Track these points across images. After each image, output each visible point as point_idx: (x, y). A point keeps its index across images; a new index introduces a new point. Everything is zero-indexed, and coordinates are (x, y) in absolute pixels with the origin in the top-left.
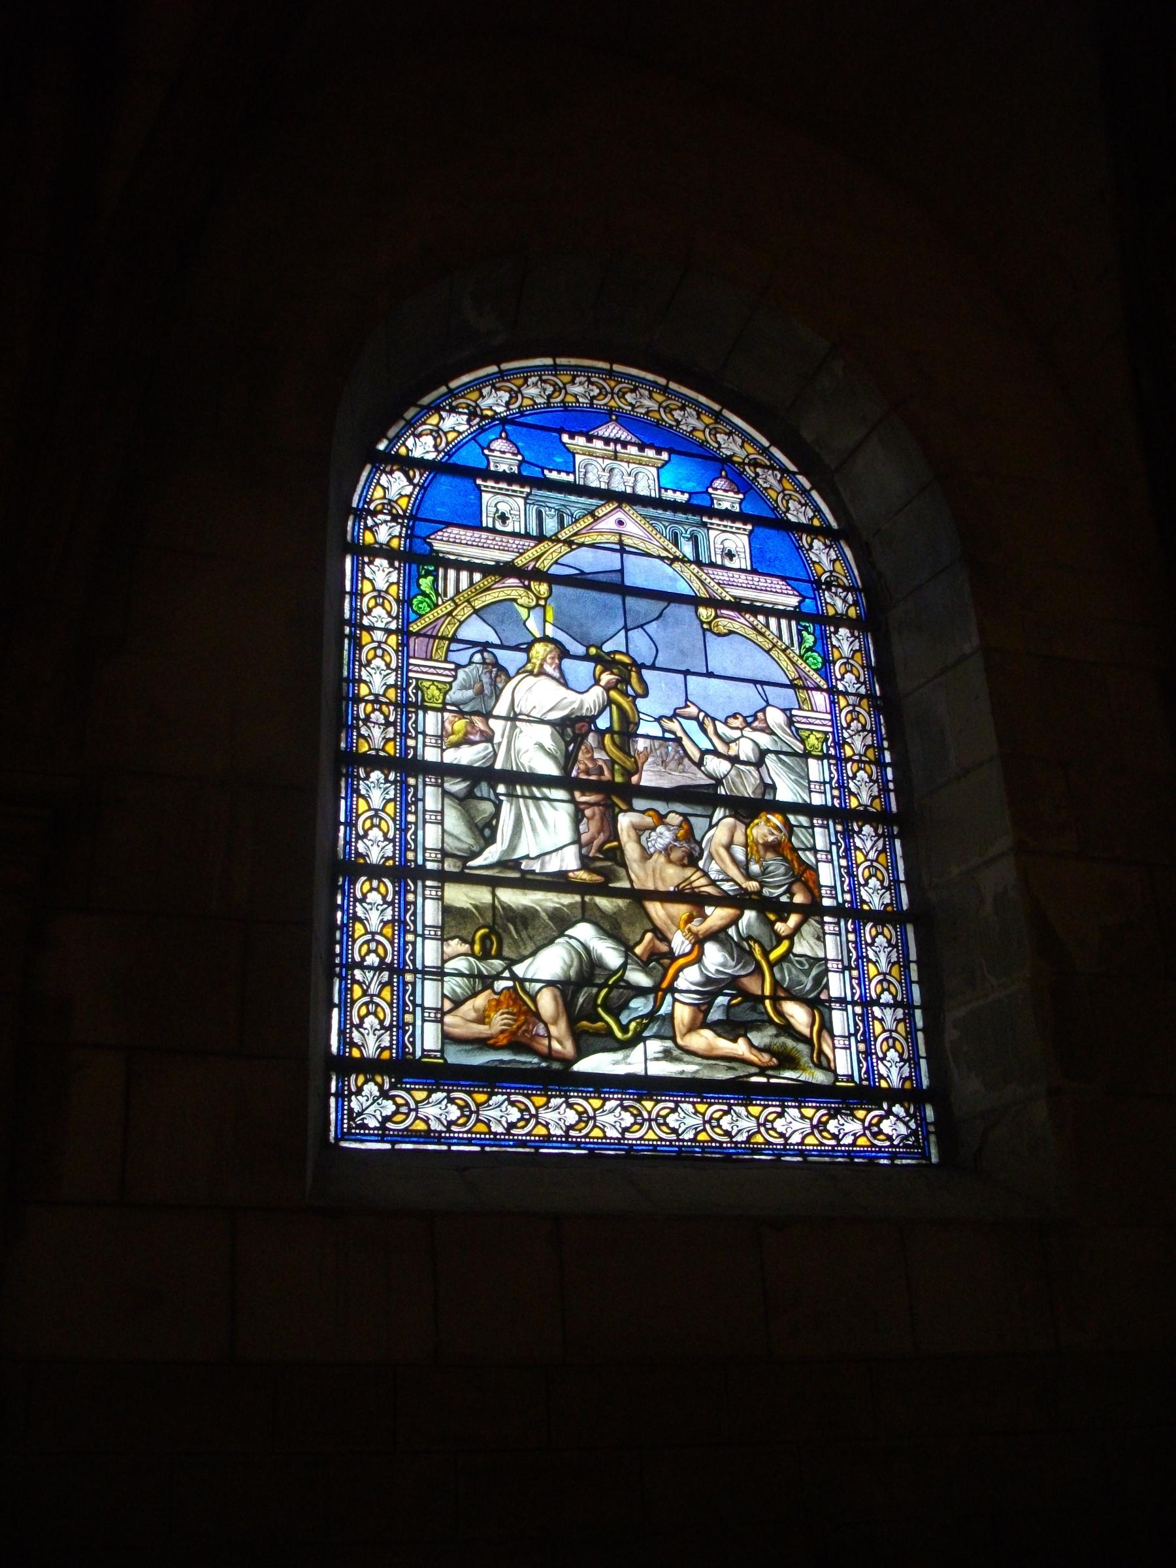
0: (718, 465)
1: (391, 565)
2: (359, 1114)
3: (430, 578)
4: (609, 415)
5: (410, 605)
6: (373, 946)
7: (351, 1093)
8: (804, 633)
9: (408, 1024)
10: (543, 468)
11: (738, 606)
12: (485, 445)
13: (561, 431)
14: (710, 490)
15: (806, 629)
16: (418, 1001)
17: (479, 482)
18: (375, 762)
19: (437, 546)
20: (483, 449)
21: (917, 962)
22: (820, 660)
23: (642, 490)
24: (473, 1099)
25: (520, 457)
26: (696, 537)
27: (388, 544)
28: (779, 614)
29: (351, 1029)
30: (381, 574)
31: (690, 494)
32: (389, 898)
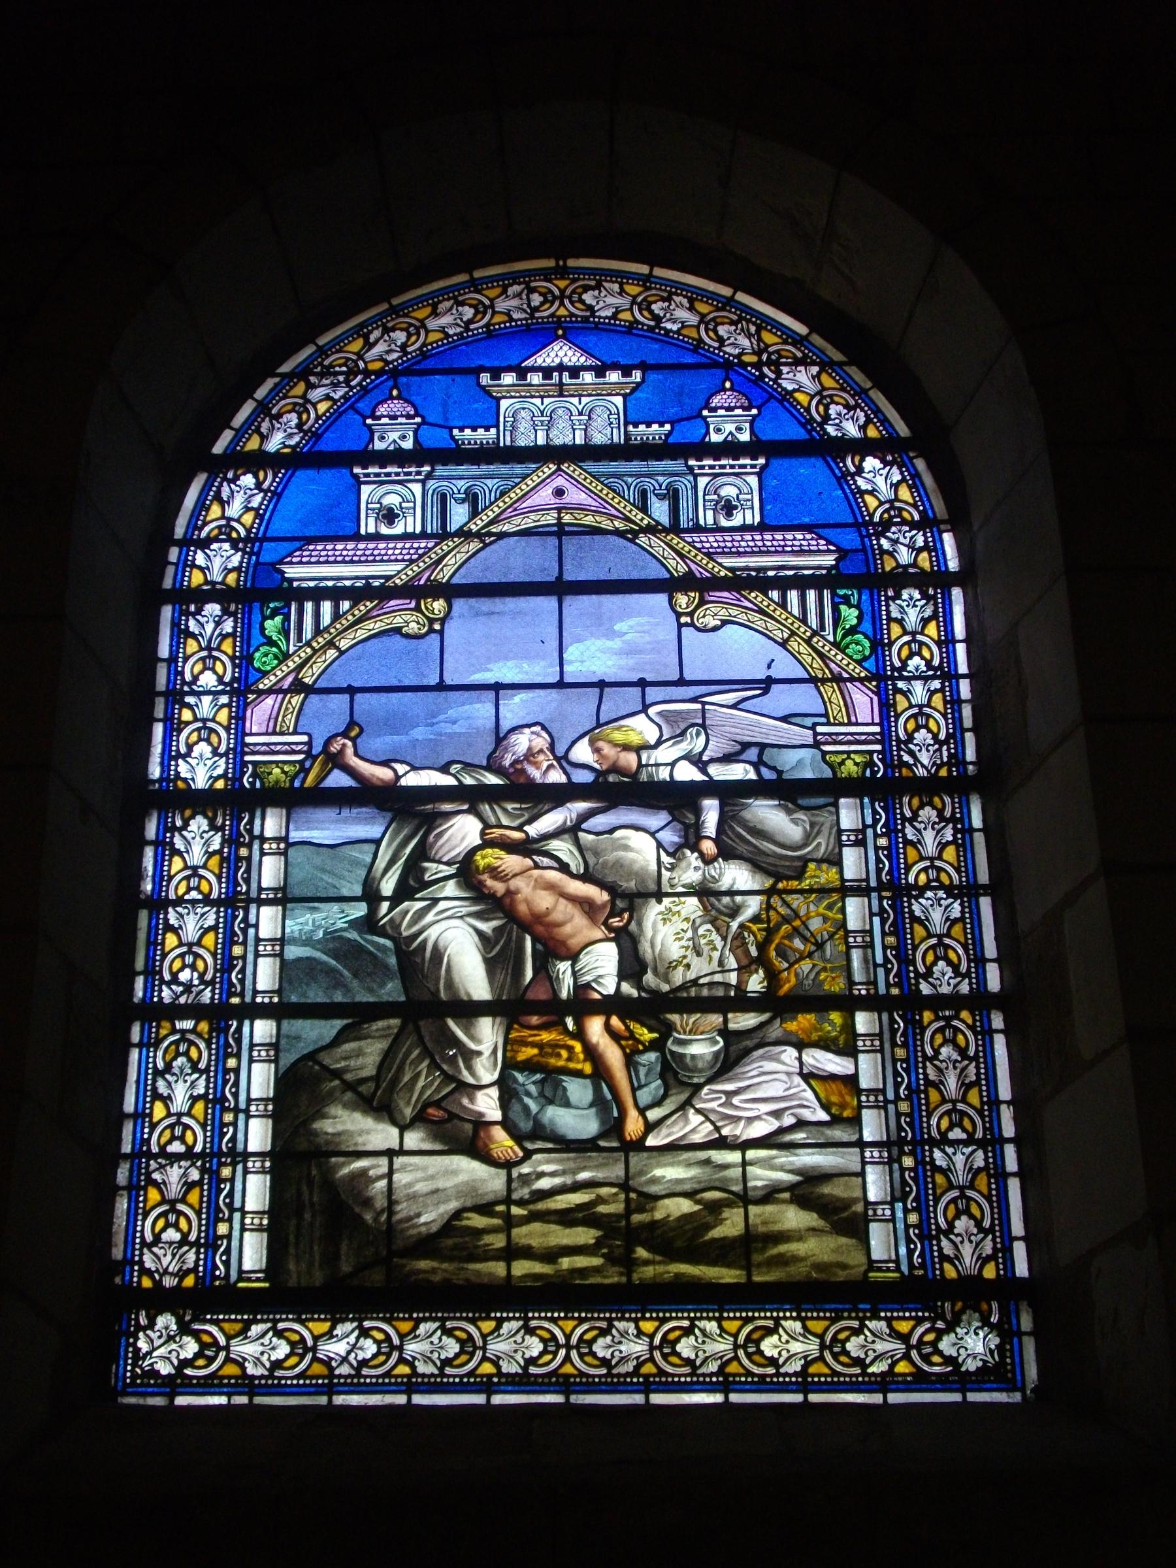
8: (843, 608)
9: (227, 1125)
10: (451, 429)
14: (705, 413)
15: (846, 600)
17: (357, 470)
20: (365, 418)
26: (676, 491)
28: (802, 583)
31: (672, 423)
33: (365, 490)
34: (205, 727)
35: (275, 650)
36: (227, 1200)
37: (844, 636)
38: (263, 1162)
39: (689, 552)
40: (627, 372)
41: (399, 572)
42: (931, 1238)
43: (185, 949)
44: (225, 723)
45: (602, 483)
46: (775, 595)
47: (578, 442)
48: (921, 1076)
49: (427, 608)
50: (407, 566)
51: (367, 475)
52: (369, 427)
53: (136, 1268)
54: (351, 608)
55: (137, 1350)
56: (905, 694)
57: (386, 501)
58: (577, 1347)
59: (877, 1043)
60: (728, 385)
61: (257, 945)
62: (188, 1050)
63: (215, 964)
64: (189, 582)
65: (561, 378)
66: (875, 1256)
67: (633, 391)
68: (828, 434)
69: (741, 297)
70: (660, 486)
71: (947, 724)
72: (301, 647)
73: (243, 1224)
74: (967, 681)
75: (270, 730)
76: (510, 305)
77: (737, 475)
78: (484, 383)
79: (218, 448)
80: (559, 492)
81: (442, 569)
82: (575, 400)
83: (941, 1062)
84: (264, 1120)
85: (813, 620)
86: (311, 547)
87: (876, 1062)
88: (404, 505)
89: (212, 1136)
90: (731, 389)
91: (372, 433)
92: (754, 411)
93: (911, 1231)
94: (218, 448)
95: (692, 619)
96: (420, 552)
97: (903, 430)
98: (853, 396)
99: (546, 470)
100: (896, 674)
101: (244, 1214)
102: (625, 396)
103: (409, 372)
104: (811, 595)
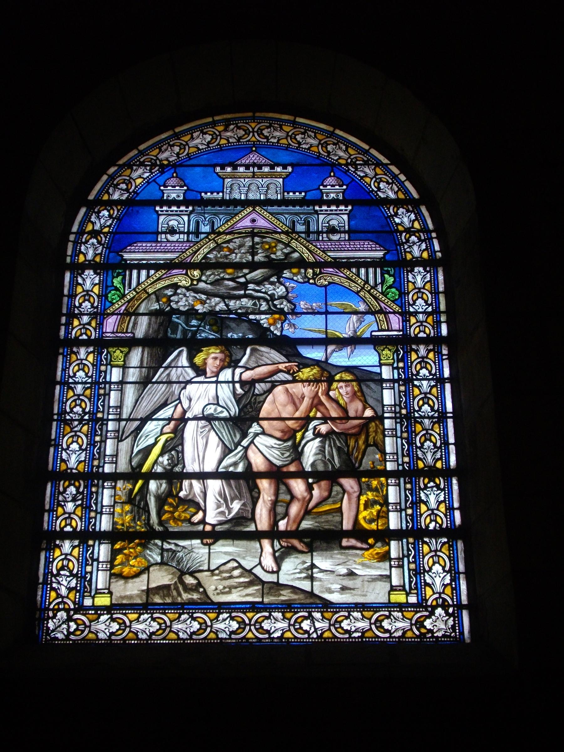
0: (330, 168)
1: (95, 273)
2: (53, 631)
3: (120, 278)
4: (249, 149)
5: (106, 297)
6: (81, 366)
7: (82, 243)
8: (386, 276)
9: (92, 518)
10: (201, 193)
11: (337, 264)
12: (162, 183)
13: (214, 166)
14: (321, 187)
15: (388, 273)
16: (95, 557)
17: (158, 208)
18: (63, 536)
19: (126, 256)
20: (160, 186)
21: (455, 418)
22: (397, 293)
23: (272, 196)
24: (128, 618)
25: (185, 188)
26: (309, 222)
27: (93, 260)
29: (62, 451)
30: (90, 280)
31: (306, 192)
32: (84, 447)
33: (162, 218)
34: (82, 363)
35: (118, 293)
36: (93, 527)
37: (387, 289)
38: (113, 458)
39: (314, 250)
40: (285, 167)
41: (177, 257)
42: (420, 573)
43: (85, 293)
44: (89, 396)
45: (274, 217)
46: (354, 270)
47: (262, 198)
48: (423, 581)
49: (191, 274)
50: (181, 255)
51: (162, 211)
52: (162, 191)
53: (49, 586)
54: (155, 273)
55: (48, 628)
56: (416, 351)
57: (171, 223)
58: (254, 625)
59: (395, 457)
60: (332, 174)
61: (107, 433)
62: (81, 404)
63: (87, 441)
64: (60, 469)
65: (254, 170)
66: (394, 583)
67: (287, 176)
68: (380, 197)
69: (338, 132)
70: (301, 219)
71: (447, 521)
72: (131, 291)
73: (98, 567)
74: (452, 420)
75: (115, 331)
76: (231, 135)
77: (337, 214)
78: (218, 171)
79: (91, 197)
80: (253, 221)
81: (197, 256)
82: (260, 180)
83: (422, 412)
84: (110, 490)
85: (371, 282)
86: (135, 245)
87: (393, 442)
88: (179, 226)
89: (83, 551)
90: (334, 176)
91: (163, 193)
92: (345, 187)
93: (408, 517)
94: (91, 197)
95: (315, 281)
96: (187, 248)
97: (415, 195)
98: (391, 179)
99: (248, 210)
100: (414, 377)
101: (99, 562)
102: (284, 179)
103: (181, 165)
104: (371, 270)
